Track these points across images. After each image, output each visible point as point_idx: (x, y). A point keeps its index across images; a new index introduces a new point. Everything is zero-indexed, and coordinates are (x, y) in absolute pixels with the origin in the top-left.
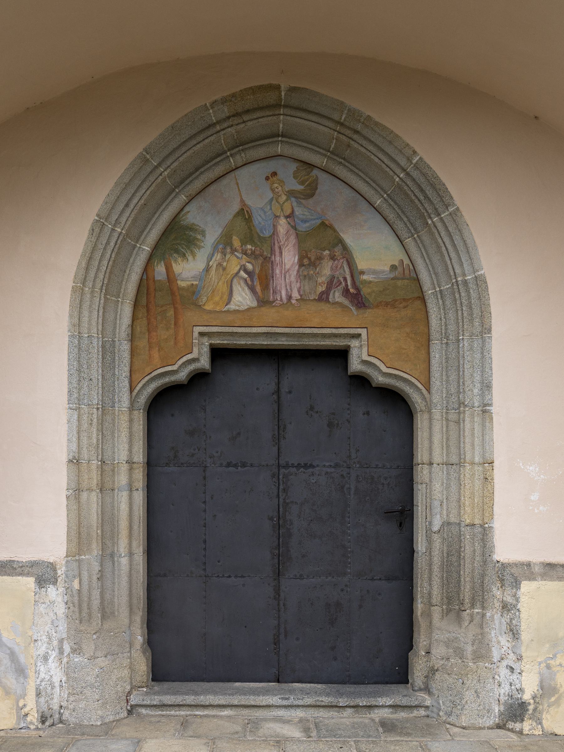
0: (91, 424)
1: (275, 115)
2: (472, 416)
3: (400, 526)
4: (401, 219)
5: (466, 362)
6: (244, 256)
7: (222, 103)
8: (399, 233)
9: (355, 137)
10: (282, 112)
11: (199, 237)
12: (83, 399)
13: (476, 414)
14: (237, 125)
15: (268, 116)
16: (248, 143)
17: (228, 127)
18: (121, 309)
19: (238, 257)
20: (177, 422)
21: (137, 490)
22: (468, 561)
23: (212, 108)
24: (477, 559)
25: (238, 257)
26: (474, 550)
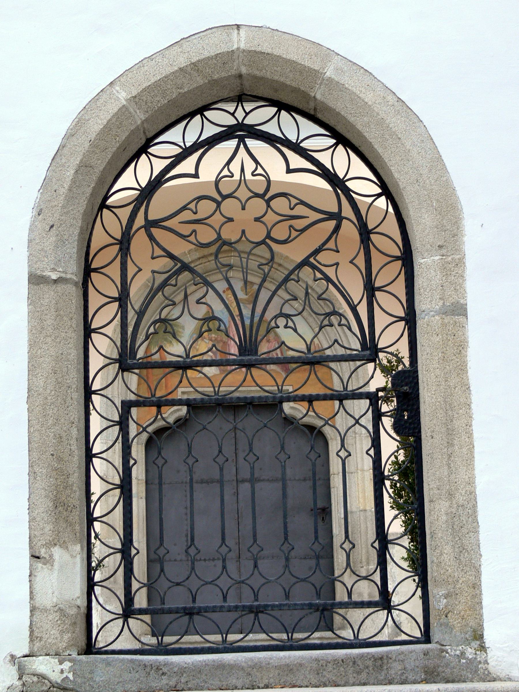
0: (115, 453)
1: (228, 257)
2: (361, 440)
3: (323, 520)
4: (312, 316)
5: (355, 405)
6: (210, 342)
7: (195, 251)
8: (311, 324)
9: (279, 268)
10: (232, 255)
11: (180, 330)
12: (109, 437)
13: (363, 438)
14: (205, 263)
15: (223, 257)
16: (211, 271)
17: (199, 264)
18: (131, 378)
19: (206, 343)
20: (173, 452)
21: (142, 498)
22: (363, 534)
23: (189, 254)
24: (369, 532)
25: (206, 343)
26: (367, 527)
